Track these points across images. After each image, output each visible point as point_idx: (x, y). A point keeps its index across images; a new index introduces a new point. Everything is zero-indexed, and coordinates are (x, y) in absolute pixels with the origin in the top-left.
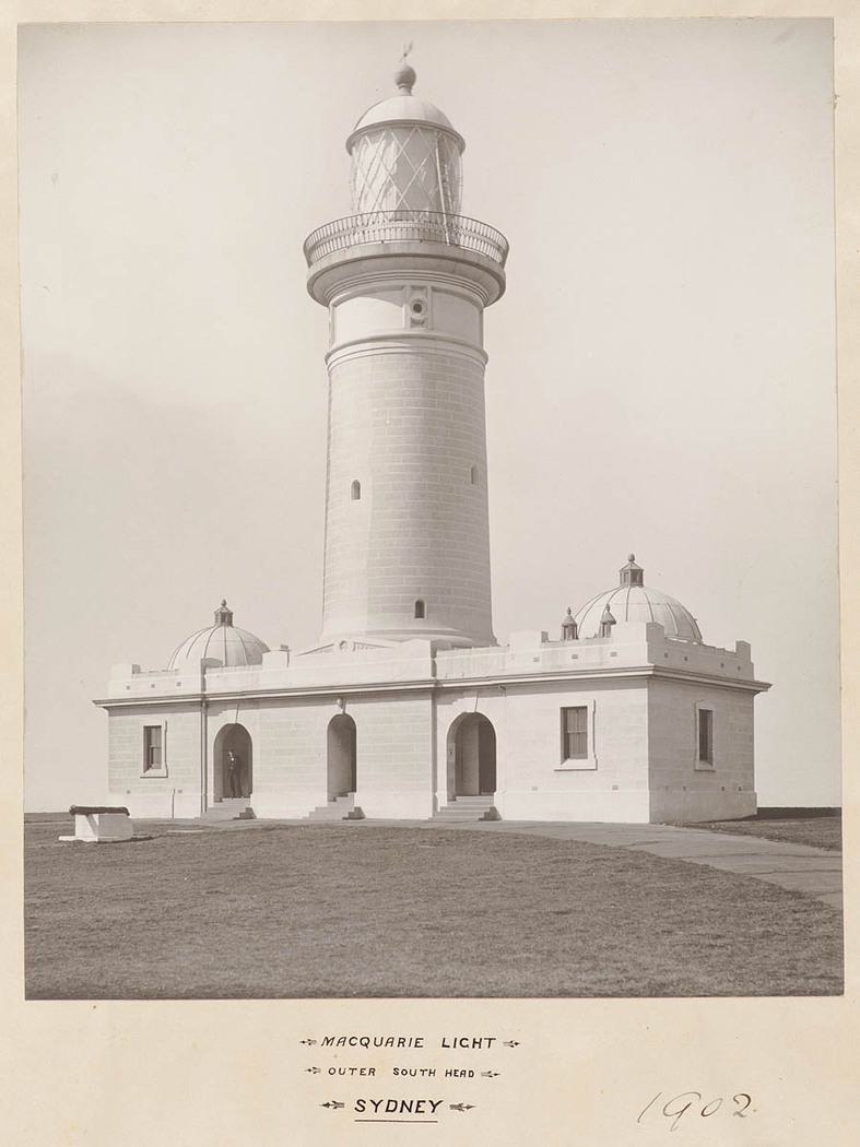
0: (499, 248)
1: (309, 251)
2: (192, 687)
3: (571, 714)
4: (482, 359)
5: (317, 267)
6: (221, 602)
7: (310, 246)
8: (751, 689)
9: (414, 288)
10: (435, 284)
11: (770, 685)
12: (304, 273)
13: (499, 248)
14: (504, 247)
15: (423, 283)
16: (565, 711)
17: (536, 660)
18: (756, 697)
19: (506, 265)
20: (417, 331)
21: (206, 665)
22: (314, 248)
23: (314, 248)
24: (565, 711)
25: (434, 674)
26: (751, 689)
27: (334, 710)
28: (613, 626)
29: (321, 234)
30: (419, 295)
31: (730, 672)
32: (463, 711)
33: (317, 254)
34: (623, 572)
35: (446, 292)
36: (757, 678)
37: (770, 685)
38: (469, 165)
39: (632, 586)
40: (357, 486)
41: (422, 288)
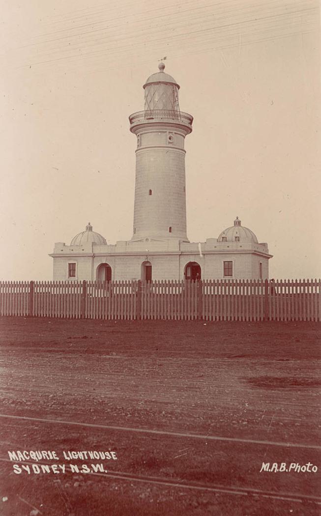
0: (190, 119)
1: (131, 120)
2: (88, 250)
3: (71, 265)
4: (184, 152)
7: (131, 118)
9: (169, 132)
10: (176, 132)
11: (272, 256)
13: (190, 119)
14: (191, 119)
16: (70, 264)
19: (193, 124)
20: (170, 145)
21: (94, 244)
22: (132, 119)
23: (132, 119)
24: (70, 264)
25: (93, 252)
26: (268, 257)
28: (66, 245)
30: (171, 135)
31: (261, 250)
32: (101, 263)
33: (133, 121)
34: (87, 227)
37: (272, 256)
38: (181, 93)
39: (89, 231)
40: (150, 194)
41: (171, 132)
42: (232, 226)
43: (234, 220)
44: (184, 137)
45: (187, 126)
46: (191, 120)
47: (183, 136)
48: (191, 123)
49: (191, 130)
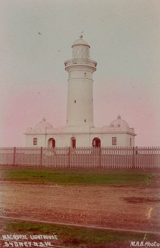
0: (95, 64)
1: (65, 64)
3: (35, 139)
5: (67, 66)
6: (43, 117)
8: (134, 135)
9: (85, 71)
10: (88, 70)
12: (65, 67)
13: (95, 64)
14: (96, 63)
15: (86, 70)
17: (108, 130)
18: (135, 137)
19: (97, 66)
21: (46, 128)
22: (66, 64)
23: (66, 64)
27: (71, 136)
29: (69, 61)
30: (85, 72)
32: (94, 137)
35: (81, 70)
36: (135, 133)
41: (86, 71)
42: (116, 119)
43: (117, 116)
44: (92, 73)
45: (94, 67)
46: (96, 65)
47: (92, 72)
48: (96, 66)
49: (96, 69)
